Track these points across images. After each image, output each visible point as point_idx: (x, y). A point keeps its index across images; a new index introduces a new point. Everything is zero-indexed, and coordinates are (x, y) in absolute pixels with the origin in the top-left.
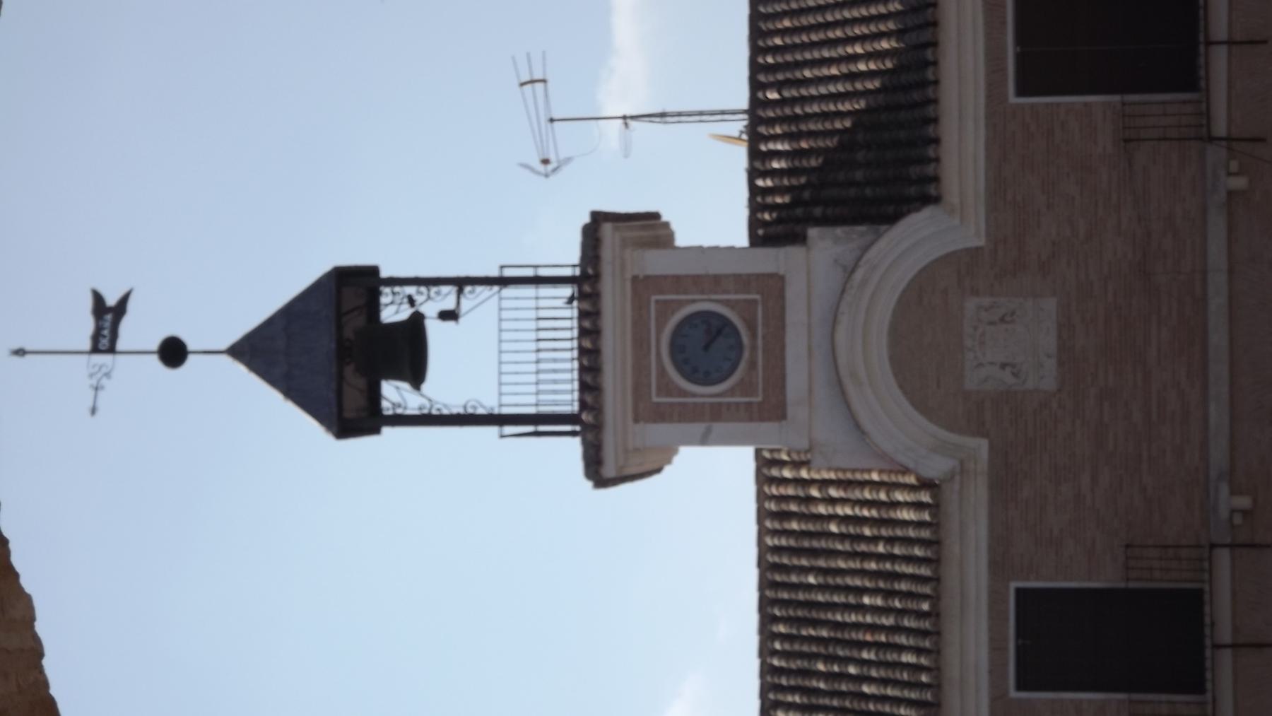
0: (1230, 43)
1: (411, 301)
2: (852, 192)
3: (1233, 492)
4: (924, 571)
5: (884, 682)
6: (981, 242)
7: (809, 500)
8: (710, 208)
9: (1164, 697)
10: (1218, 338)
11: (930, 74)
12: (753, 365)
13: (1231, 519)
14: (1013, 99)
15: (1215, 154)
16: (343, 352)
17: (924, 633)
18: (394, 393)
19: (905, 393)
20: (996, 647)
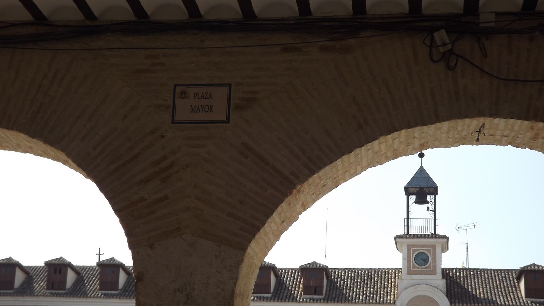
2: (452, 288)
4: (378, 301)
8: (450, 260)
12: (418, 268)
16: (421, 188)
18: (413, 198)
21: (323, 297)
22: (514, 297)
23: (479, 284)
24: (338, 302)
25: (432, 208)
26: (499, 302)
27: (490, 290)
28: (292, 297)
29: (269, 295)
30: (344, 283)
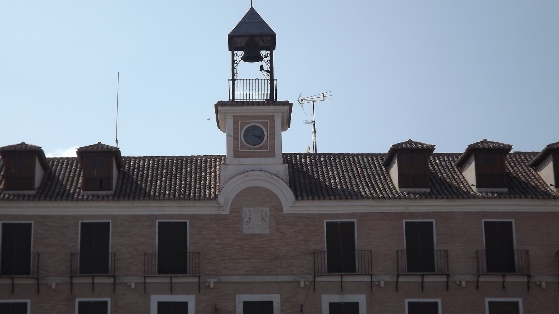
0: (342, 282)
1: (266, 57)
2: (297, 179)
3: (214, 282)
4: (192, 196)
5: (160, 187)
6: (284, 212)
7: (211, 169)
8: (294, 141)
9: (157, 263)
10: (258, 279)
11: (332, 197)
12: (249, 148)
13: (207, 282)
14: (325, 221)
15: (310, 278)
16: (252, 37)
17: (174, 196)
18: (240, 54)
19: (242, 191)
20: (171, 216)
21: (112, 192)
22: (384, 188)
23: (333, 173)
24: (134, 199)
25: (267, 67)
26: (363, 193)
27: (350, 179)
28: (66, 194)
29: (33, 192)
30: (142, 175)
